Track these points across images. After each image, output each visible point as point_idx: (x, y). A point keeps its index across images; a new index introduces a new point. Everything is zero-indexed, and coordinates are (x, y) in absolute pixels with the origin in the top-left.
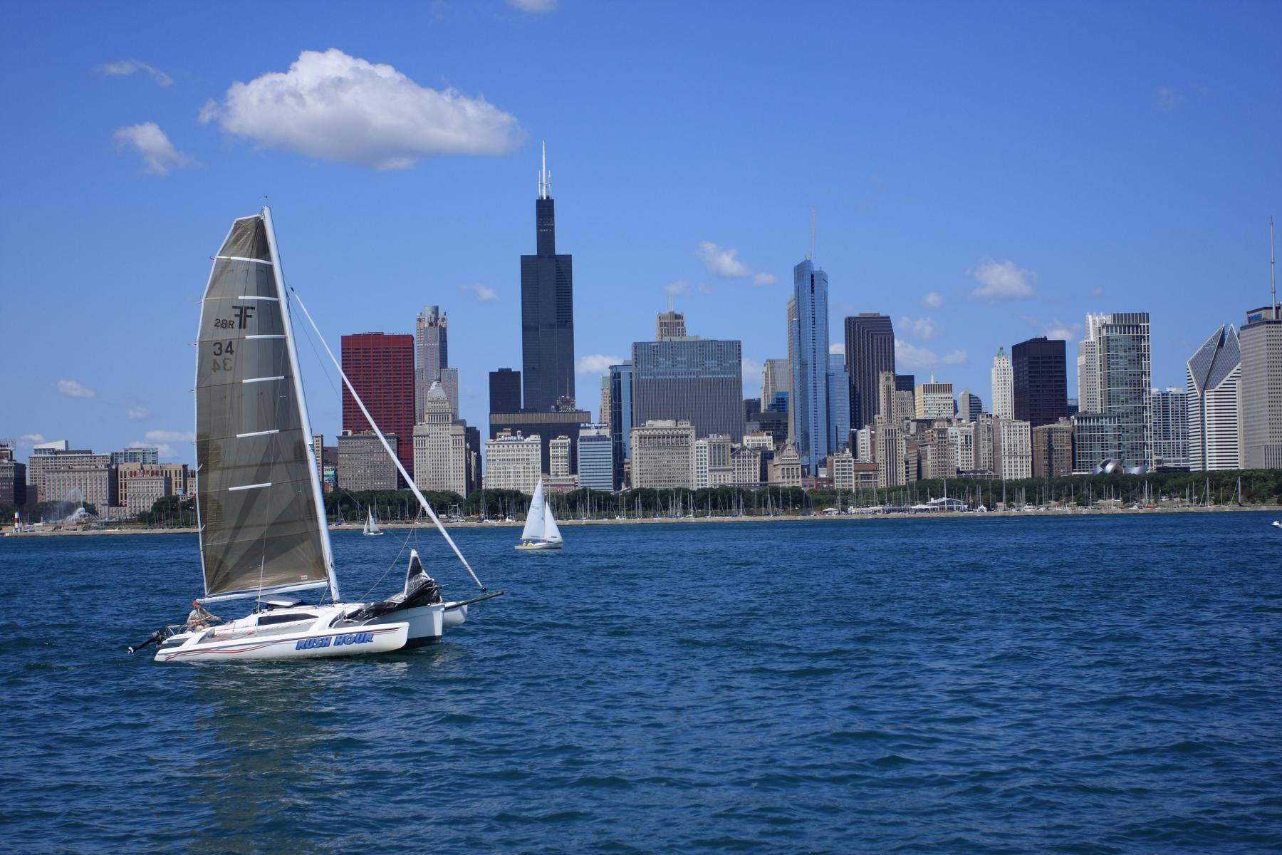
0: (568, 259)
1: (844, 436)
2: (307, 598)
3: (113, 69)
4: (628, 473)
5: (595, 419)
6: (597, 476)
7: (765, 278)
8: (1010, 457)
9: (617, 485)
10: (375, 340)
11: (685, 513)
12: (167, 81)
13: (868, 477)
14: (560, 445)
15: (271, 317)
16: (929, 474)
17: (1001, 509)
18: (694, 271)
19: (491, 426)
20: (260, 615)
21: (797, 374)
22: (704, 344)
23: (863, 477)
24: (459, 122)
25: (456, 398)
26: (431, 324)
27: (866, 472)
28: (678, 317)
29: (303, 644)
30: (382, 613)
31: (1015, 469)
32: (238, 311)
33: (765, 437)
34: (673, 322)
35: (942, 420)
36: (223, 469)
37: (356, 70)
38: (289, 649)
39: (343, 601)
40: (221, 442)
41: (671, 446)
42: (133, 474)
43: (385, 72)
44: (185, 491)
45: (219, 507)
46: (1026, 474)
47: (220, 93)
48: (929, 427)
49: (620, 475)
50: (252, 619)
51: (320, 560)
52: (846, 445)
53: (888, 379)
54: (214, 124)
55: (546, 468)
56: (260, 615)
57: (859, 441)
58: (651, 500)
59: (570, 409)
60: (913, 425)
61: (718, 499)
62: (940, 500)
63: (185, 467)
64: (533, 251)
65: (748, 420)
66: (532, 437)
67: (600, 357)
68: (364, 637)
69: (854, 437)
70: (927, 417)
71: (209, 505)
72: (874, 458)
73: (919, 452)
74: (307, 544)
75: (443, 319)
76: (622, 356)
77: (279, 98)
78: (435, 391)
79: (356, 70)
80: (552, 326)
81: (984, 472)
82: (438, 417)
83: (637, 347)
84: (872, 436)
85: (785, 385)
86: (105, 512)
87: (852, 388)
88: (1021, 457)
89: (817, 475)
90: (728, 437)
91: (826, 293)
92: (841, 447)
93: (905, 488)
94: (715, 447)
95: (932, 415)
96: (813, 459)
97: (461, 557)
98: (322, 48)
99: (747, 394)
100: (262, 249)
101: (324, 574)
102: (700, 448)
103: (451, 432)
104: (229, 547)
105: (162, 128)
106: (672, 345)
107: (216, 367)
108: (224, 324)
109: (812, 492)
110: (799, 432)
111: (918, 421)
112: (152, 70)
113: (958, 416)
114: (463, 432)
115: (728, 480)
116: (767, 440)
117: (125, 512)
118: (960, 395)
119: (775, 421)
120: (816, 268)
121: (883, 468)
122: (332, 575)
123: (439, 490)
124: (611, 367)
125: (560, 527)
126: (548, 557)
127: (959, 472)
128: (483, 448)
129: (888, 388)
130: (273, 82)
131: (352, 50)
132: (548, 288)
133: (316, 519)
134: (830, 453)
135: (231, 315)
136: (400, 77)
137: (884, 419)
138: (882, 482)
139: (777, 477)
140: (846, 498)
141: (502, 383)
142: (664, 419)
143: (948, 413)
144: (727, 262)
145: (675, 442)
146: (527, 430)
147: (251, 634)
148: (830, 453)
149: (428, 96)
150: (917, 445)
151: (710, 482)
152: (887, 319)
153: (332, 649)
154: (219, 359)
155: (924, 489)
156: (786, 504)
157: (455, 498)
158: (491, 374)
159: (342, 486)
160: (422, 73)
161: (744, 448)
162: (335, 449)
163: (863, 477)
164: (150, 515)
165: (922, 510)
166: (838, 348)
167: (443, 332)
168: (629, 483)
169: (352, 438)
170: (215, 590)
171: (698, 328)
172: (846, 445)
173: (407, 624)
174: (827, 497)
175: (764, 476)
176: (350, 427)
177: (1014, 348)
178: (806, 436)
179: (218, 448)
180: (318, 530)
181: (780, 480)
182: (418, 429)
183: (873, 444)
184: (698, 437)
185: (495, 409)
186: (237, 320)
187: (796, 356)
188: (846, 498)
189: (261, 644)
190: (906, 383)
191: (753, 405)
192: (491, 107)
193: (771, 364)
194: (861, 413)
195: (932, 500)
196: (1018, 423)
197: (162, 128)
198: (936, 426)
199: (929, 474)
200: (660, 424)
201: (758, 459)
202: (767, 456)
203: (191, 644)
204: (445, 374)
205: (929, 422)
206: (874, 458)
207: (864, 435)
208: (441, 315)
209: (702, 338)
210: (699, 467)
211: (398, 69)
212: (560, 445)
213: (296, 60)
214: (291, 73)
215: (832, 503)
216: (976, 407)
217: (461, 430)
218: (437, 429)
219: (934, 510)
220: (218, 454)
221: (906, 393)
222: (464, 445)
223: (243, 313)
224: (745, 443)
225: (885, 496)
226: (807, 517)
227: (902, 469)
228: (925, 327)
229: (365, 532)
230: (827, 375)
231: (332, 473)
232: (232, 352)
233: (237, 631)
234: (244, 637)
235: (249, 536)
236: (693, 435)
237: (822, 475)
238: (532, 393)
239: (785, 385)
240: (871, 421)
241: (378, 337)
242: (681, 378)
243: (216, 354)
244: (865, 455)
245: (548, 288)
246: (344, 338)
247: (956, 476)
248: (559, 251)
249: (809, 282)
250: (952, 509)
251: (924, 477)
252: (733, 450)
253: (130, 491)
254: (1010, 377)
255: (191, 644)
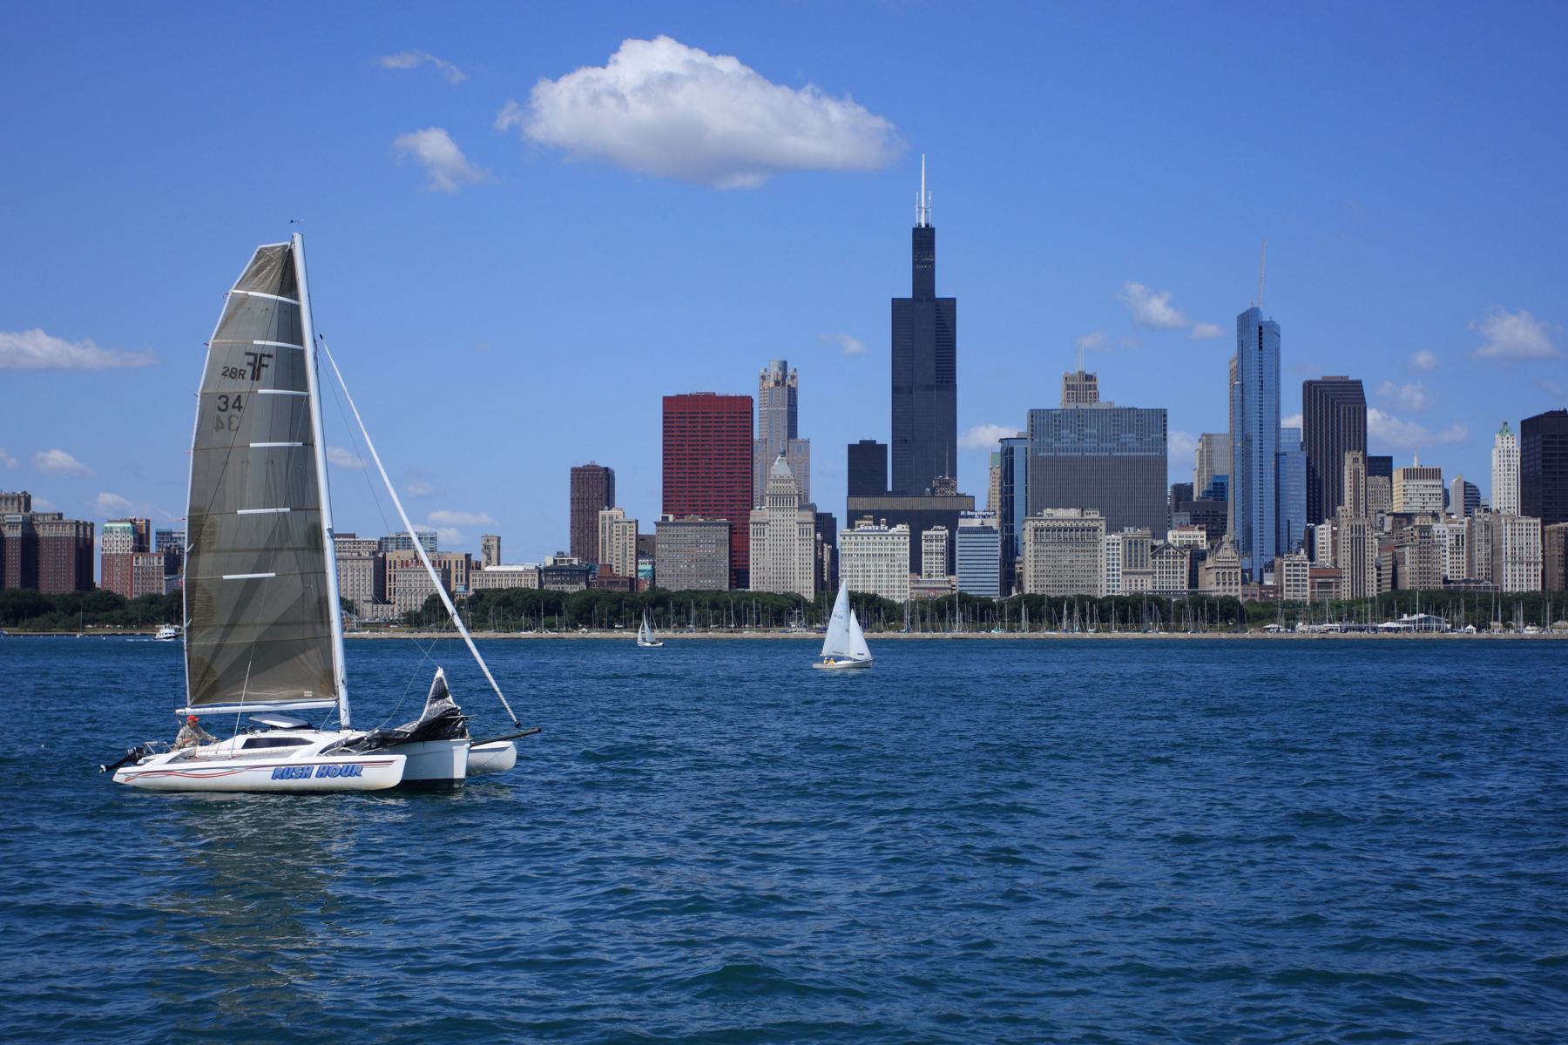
0: (952, 302)
1: (1298, 533)
2: (313, 720)
3: (392, 62)
4: (1020, 575)
5: (981, 505)
6: (983, 581)
7: (1208, 329)
8: (1514, 564)
9: (1006, 587)
10: (707, 401)
11: (1083, 630)
12: (458, 76)
13: (1328, 585)
14: (934, 539)
15: (293, 370)
16: (1406, 583)
17: (1496, 631)
18: (1114, 318)
19: (849, 512)
20: (249, 736)
21: (1238, 452)
22: (1119, 413)
23: (1321, 585)
24: (820, 128)
25: (807, 476)
26: (777, 383)
27: (1325, 580)
28: (1089, 378)
29: (280, 773)
30: (386, 743)
31: (1520, 579)
32: (251, 359)
33: (1197, 533)
34: (1082, 385)
35: (1426, 514)
36: (218, 551)
37: (691, 63)
38: (264, 779)
39: (353, 726)
40: (217, 518)
41: (1076, 542)
42: (405, 564)
43: (728, 65)
44: (467, 587)
45: (210, 599)
46: (1535, 586)
47: (523, 96)
48: (1409, 523)
49: (1010, 577)
50: (241, 739)
51: (330, 674)
52: (1301, 544)
53: (1356, 460)
54: (515, 131)
55: (916, 566)
56: (249, 736)
57: (1317, 540)
58: (1043, 610)
59: (949, 492)
60: (1388, 520)
61: (1127, 610)
62: (1415, 617)
63: (468, 556)
64: (907, 293)
65: (1177, 510)
66: (899, 527)
67: (994, 428)
68: (351, 770)
69: (1311, 534)
70: (1408, 510)
71: (198, 595)
72: (1336, 562)
73: (1394, 555)
74: (312, 653)
75: (793, 377)
76: (1015, 429)
77: (595, 99)
78: (780, 468)
79: (691, 63)
80: (929, 388)
81: (1480, 582)
82: (779, 500)
83: (1034, 415)
84: (1334, 533)
85: (1224, 466)
86: (368, 611)
87: (1311, 471)
88: (1529, 564)
89: (1261, 582)
90: (1148, 532)
91: (1277, 350)
92: (1294, 547)
93: (1372, 600)
94: (1131, 544)
95: (1415, 507)
96: (1257, 562)
97: (488, 675)
98: (649, 36)
99: (1174, 477)
100: (288, 284)
101: (332, 691)
102: (1111, 545)
103: (797, 518)
104: (219, 647)
105: (452, 135)
106: (1079, 415)
107: (219, 425)
108: (233, 373)
109: (1252, 603)
110: (1239, 528)
111: (1395, 515)
112: (439, 63)
113: (1448, 510)
114: (811, 519)
115: (1147, 585)
116: (1199, 536)
117: (393, 612)
118: (1452, 483)
119: (1209, 510)
120: (1265, 318)
121: (1347, 574)
122: (343, 693)
123: (780, 591)
124: (1001, 441)
125: (869, 642)
126: (852, 683)
127: (1446, 581)
128: (839, 539)
129: (1356, 473)
130: (588, 80)
131: (688, 38)
132: (925, 339)
133: (329, 623)
134: (1278, 554)
135: (242, 363)
136: (745, 71)
137: (1350, 512)
138: (1345, 593)
139: (1211, 585)
140: (1293, 612)
141: (863, 459)
142: (1068, 507)
143: (1435, 505)
144: (1158, 309)
145: (1080, 536)
146: (893, 518)
147: (240, 757)
148: (1278, 554)
149: (781, 95)
150: (1393, 544)
151: (1123, 588)
152: (1358, 384)
153: (313, 782)
154: (224, 416)
155: (1394, 602)
156: (1212, 620)
157: (798, 601)
158: (851, 448)
159: (659, 585)
160: (774, 63)
161: (1168, 546)
162: (653, 537)
163: (1321, 585)
164: (418, 615)
165: (1389, 629)
166: (1293, 421)
167: (792, 393)
168: (1020, 588)
169: (673, 524)
170: (198, 702)
171: (1114, 393)
172: (1301, 544)
173: (404, 757)
174: (1262, 612)
175: (1194, 581)
176: (672, 511)
177: (1525, 424)
178: (1248, 532)
179: (213, 525)
180: (329, 637)
181: (1213, 587)
182: (755, 515)
183: (1335, 543)
184: (1109, 531)
185: (854, 490)
186: (249, 370)
187: (1238, 429)
188: (1293, 612)
189: (232, 770)
190: (1381, 466)
191: (1183, 491)
192: (861, 110)
193: (1207, 439)
194: (1319, 507)
195: (1405, 617)
196: (1524, 520)
197: (451, 135)
198: (1417, 521)
199: (1406, 583)
200: (1060, 513)
201: (1186, 561)
202: (1198, 557)
203: (157, 768)
204: (793, 445)
205: (1409, 517)
206: (1336, 562)
207: (1323, 532)
208: (790, 372)
209: (1117, 405)
210: (1110, 569)
211: (744, 61)
212: (934, 539)
213: (616, 50)
214: (611, 67)
215: (1272, 617)
216: (1472, 498)
217: (808, 516)
218: (779, 515)
219: (1408, 629)
220: (213, 533)
221: (1380, 479)
222: (812, 535)
223: (258, 362)
224: (1170, 539)
225: (1348, 611)
226: (1240, 635)
227: (1372, 575)
228: (1414, 395)
229: (640, 642)
230: (1277, 455)
231: (649, 567)
232: (239, 408)
233: (220, 753)
234: (226, 763)
235: (245, 637)
236: (1103, 528)
237: (1268, 583)
238: (903, 471)
239: (1224, 466)
240: (1333, 514)
241: (709, 399)
242: (1093, 455)
243: (222, 410)
244: (1324, 557)
245: (925, 339)
246: (666, 399)
247: (1442, 587)
248: (940, 292)
249: (1257, 336)
250: (1427, 629)
251: (1400, 587)
252: (1153, 548)
253: (400, 585)
254: (1516, 460)
255: (157, 768)
